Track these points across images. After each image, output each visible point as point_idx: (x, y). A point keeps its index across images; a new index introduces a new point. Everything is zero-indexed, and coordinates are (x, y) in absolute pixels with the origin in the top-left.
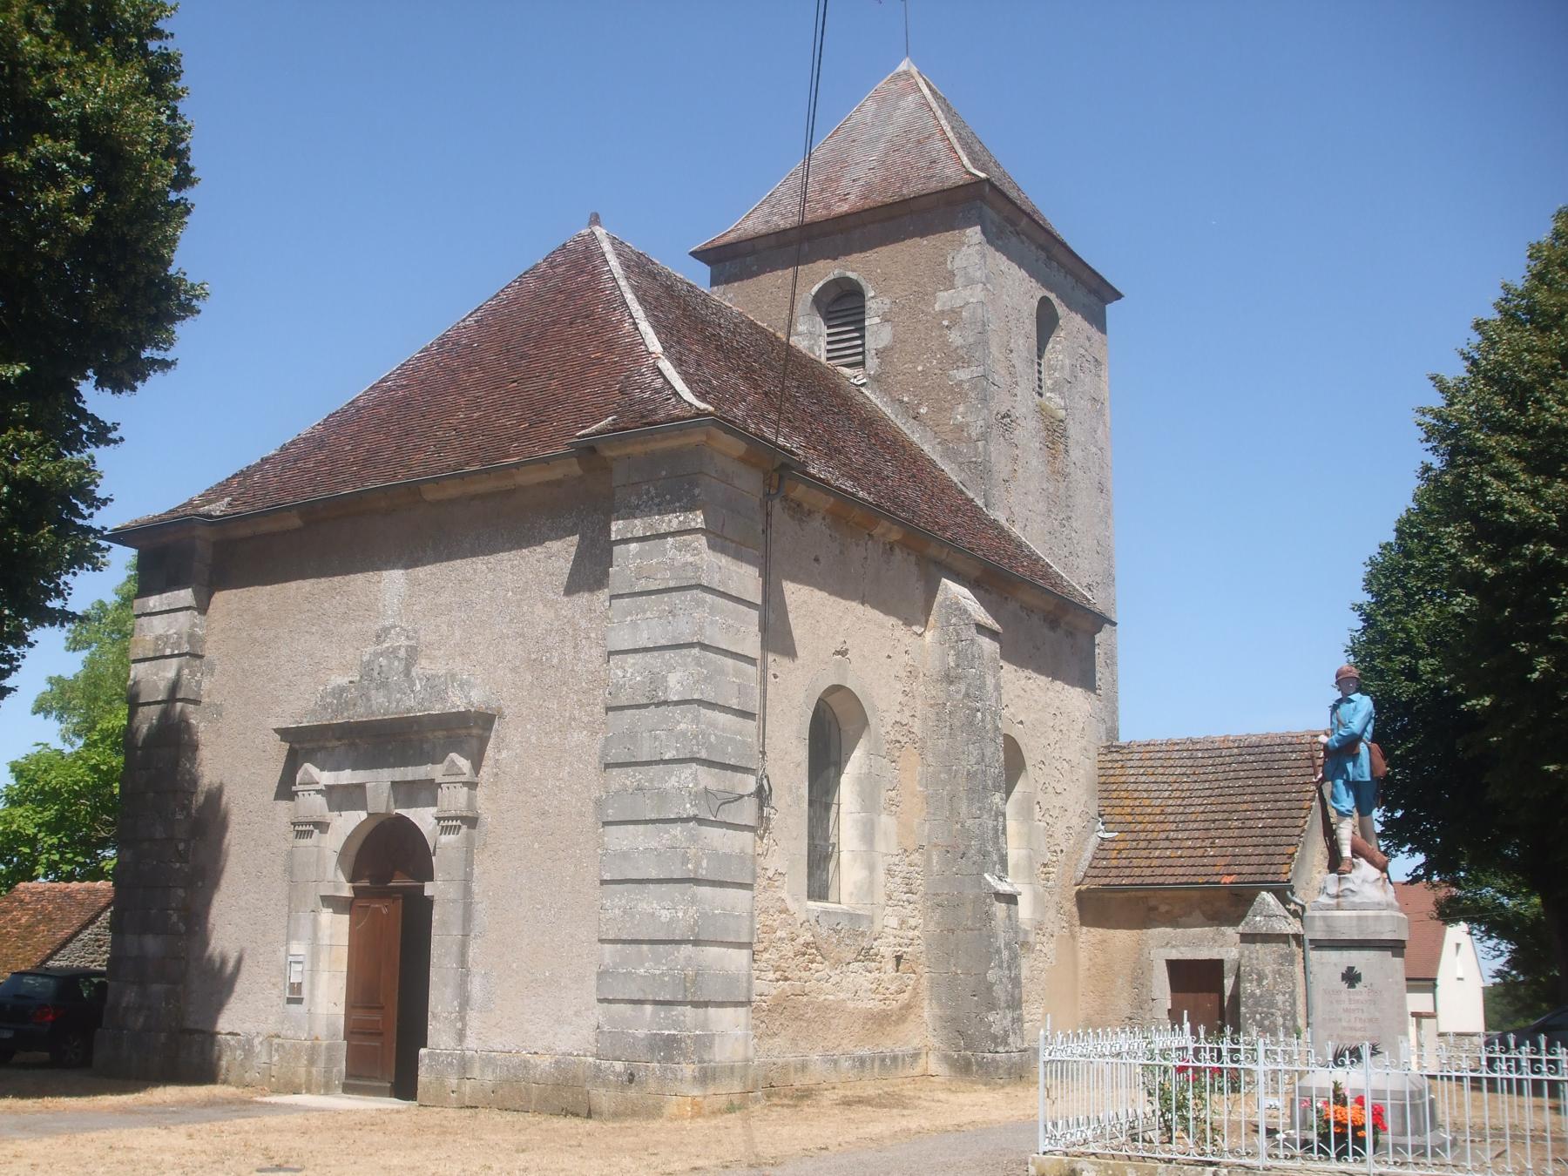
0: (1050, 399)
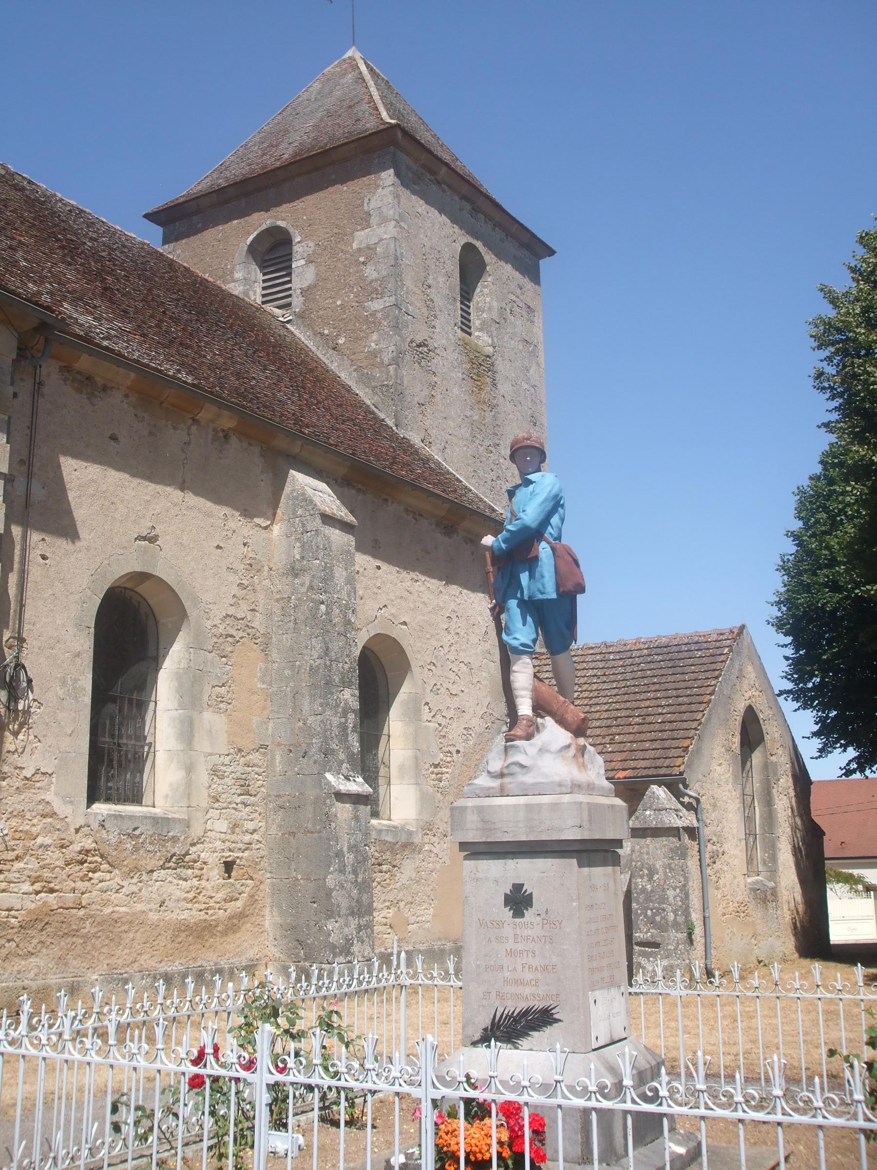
0: (478, 337)
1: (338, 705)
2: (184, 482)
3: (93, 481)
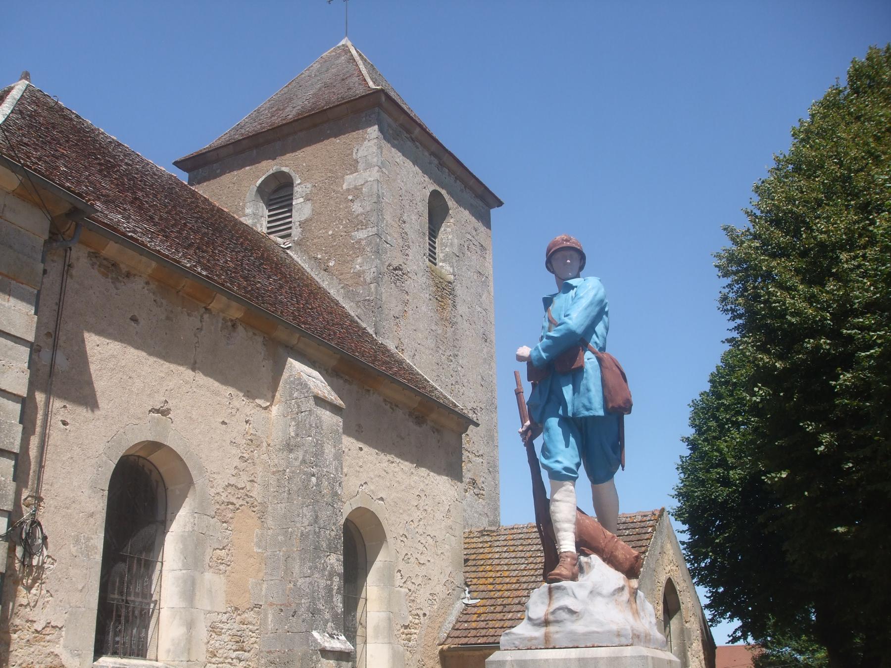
1: (324, 569)
2: (195, 363)
3: (113, 356)
